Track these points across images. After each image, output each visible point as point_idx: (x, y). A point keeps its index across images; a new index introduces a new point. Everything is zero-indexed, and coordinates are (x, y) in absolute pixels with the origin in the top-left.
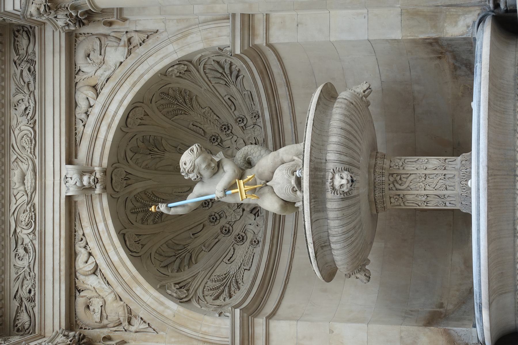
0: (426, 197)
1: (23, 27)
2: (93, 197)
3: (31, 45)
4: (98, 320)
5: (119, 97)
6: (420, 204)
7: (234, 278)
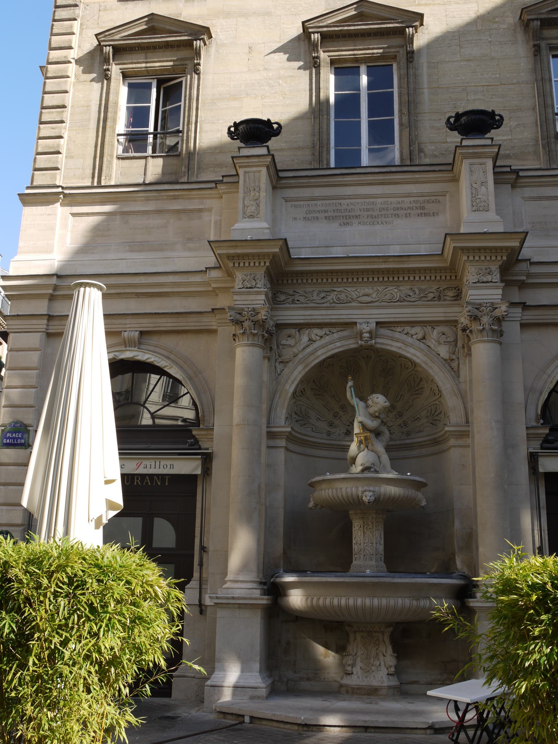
1: (461, 293)
4: (282, 343)
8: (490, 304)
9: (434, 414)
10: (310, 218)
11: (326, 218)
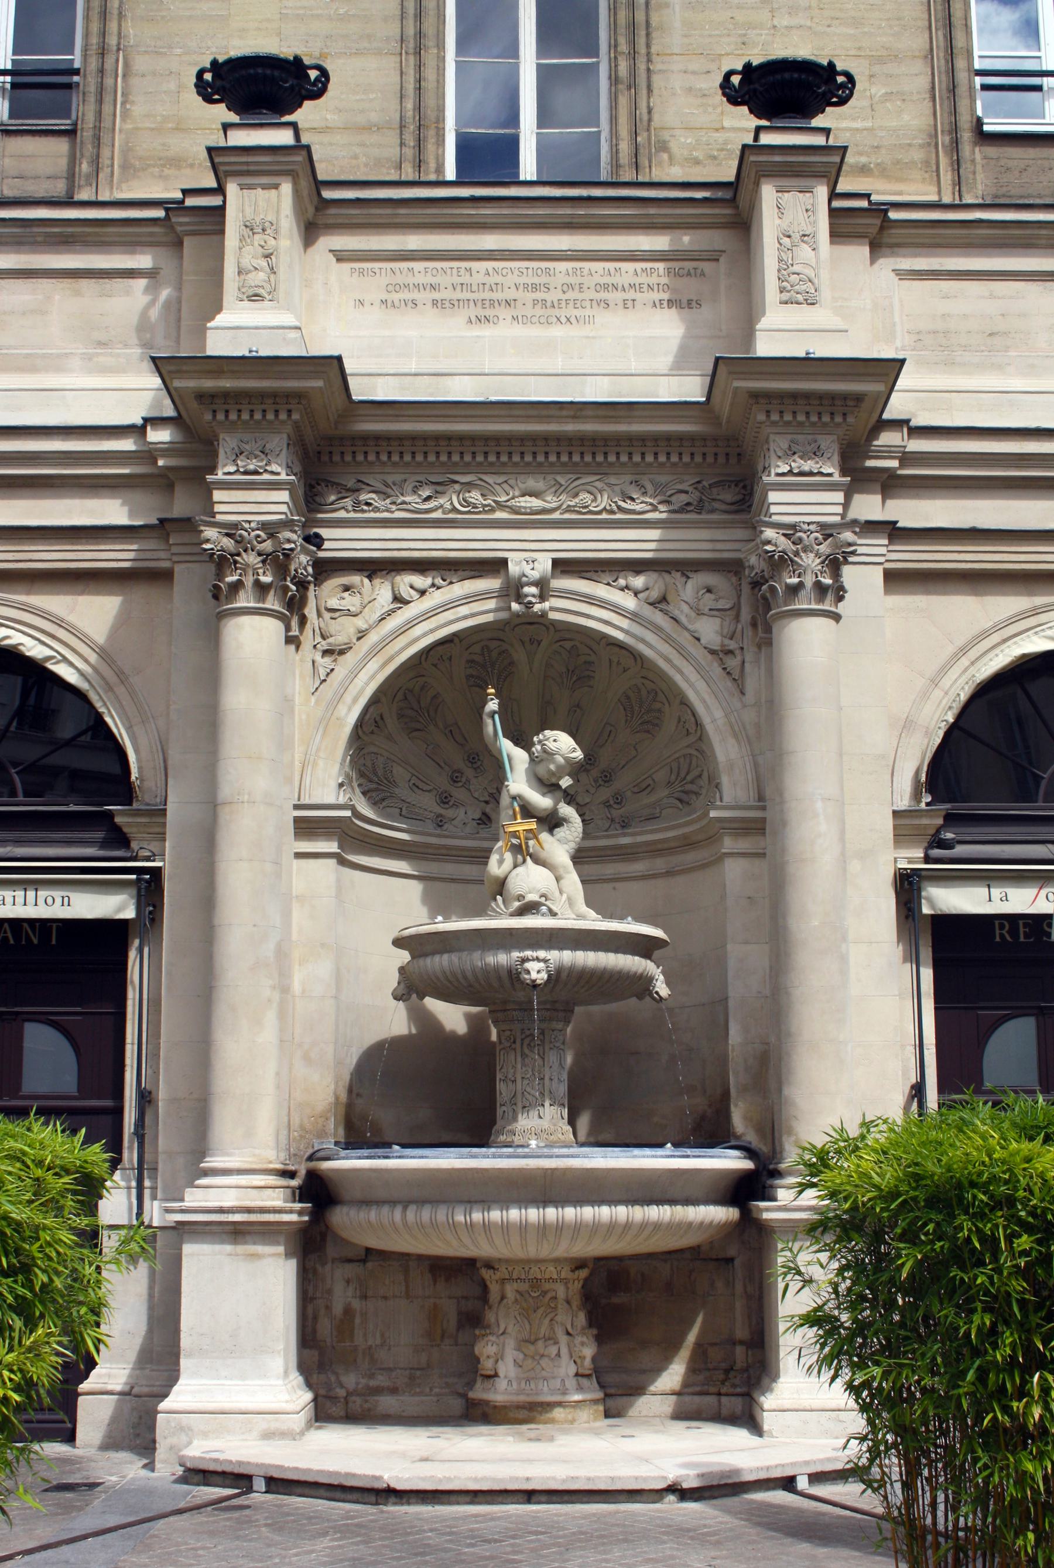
3: (724, 507)
5: (649, 636)
9: (685, 778)
10: (397, 303)
11: (435, 303)
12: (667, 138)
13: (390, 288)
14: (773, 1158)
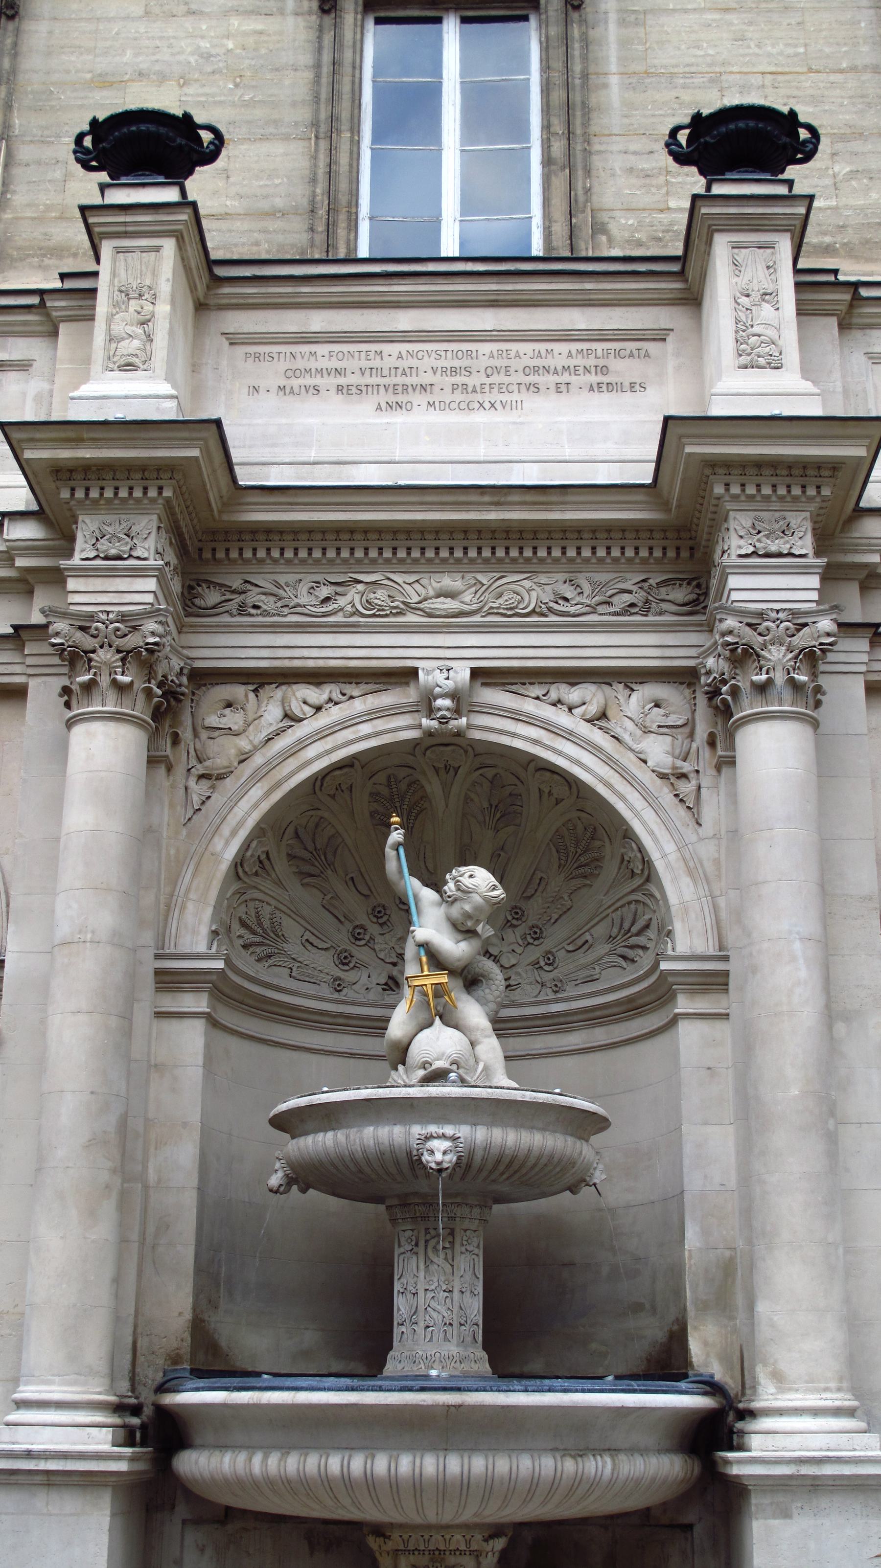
0: (414, 1291)
1: (706, 594)
2: (416, 714)
3: (674, 608)
6: (402, 1280)
7: (276, 951)
8: (786, 613)
9: (629, 931)
10: (296, 390)
11: (339, 389)
12: (606, 220)
13: (289, 373)
14: (743, 1394)
